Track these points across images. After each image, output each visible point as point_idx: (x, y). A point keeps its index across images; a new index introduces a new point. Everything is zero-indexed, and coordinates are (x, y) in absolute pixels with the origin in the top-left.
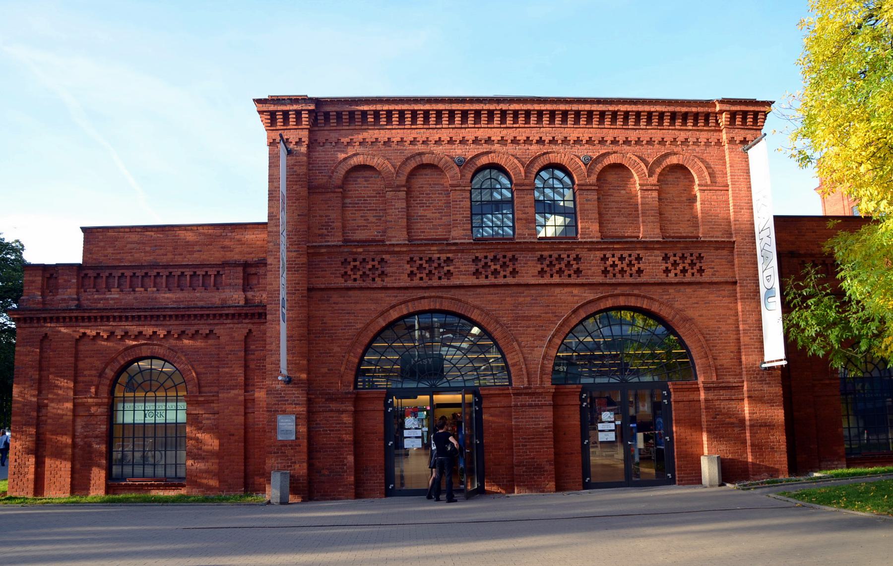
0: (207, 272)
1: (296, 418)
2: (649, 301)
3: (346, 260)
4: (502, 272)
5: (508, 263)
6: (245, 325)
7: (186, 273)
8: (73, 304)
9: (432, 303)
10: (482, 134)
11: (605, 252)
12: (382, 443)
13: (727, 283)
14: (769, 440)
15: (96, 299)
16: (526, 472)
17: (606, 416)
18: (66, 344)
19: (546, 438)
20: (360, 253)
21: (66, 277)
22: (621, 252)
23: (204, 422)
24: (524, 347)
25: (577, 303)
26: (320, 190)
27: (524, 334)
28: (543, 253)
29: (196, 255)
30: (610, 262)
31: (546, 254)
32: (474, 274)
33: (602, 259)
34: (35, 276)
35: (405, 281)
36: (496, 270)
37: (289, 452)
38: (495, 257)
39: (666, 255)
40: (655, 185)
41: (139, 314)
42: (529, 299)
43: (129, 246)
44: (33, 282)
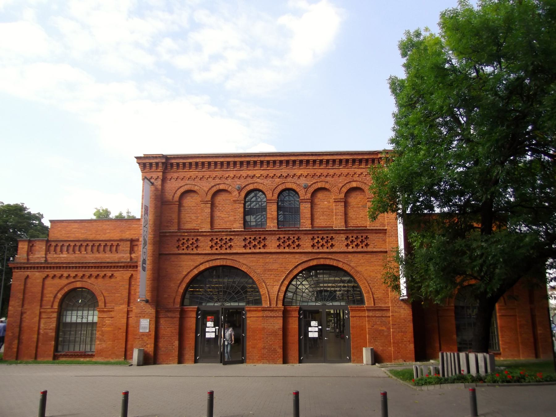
0: (112, 244)
1: (150, 320)
2: (337, 261)
3: (179, 239)
4: (258, 246)
5: (262, 241)
6: (130, 272)
7: (101, 244)
8: (43, 260)
9: (221, 262)
10: (250, 173)
11: (313, 235)
12: (194, 335)
13: (381, 252)
14: (403, 340)
15: (54, 257)
16: (267, 352)
17: (314, 323)
18: (38, 281)
19: (279, 334)
20: (186, 236)
21: (40, 246)
22: (323, 235)
23: (106, 322)
24: (269, 285)
25: (298, 262)
26: (168, 203)
27: (269, 278)
28: (280, 236)
29: (107, 235)
30: (316, 241)
31: (282, 236)
32: (244, 247)
33: (312, 239)
34: (24, 245)
35: (209, 251)
36: (255, 245)
37: (145, 338)
38: (255, 238)
39: (348, 237)
40: (343, 199)
41: (76, 265)
42: (272, 260)
43: (74, 230)
44: (23, 248)
